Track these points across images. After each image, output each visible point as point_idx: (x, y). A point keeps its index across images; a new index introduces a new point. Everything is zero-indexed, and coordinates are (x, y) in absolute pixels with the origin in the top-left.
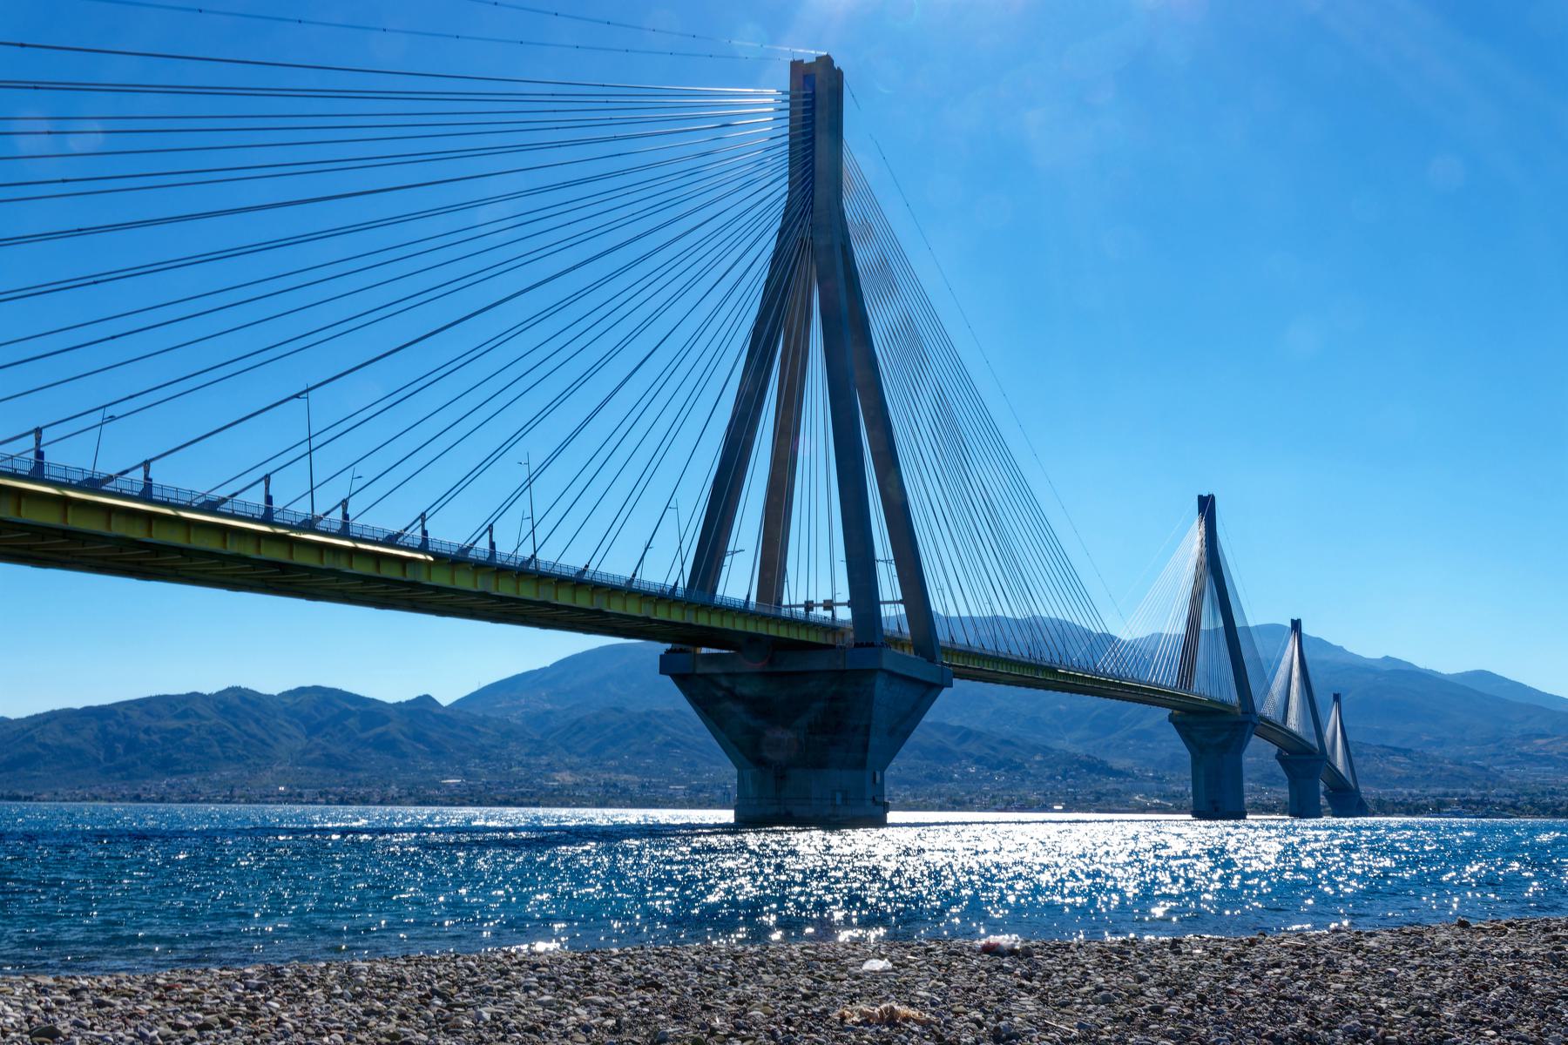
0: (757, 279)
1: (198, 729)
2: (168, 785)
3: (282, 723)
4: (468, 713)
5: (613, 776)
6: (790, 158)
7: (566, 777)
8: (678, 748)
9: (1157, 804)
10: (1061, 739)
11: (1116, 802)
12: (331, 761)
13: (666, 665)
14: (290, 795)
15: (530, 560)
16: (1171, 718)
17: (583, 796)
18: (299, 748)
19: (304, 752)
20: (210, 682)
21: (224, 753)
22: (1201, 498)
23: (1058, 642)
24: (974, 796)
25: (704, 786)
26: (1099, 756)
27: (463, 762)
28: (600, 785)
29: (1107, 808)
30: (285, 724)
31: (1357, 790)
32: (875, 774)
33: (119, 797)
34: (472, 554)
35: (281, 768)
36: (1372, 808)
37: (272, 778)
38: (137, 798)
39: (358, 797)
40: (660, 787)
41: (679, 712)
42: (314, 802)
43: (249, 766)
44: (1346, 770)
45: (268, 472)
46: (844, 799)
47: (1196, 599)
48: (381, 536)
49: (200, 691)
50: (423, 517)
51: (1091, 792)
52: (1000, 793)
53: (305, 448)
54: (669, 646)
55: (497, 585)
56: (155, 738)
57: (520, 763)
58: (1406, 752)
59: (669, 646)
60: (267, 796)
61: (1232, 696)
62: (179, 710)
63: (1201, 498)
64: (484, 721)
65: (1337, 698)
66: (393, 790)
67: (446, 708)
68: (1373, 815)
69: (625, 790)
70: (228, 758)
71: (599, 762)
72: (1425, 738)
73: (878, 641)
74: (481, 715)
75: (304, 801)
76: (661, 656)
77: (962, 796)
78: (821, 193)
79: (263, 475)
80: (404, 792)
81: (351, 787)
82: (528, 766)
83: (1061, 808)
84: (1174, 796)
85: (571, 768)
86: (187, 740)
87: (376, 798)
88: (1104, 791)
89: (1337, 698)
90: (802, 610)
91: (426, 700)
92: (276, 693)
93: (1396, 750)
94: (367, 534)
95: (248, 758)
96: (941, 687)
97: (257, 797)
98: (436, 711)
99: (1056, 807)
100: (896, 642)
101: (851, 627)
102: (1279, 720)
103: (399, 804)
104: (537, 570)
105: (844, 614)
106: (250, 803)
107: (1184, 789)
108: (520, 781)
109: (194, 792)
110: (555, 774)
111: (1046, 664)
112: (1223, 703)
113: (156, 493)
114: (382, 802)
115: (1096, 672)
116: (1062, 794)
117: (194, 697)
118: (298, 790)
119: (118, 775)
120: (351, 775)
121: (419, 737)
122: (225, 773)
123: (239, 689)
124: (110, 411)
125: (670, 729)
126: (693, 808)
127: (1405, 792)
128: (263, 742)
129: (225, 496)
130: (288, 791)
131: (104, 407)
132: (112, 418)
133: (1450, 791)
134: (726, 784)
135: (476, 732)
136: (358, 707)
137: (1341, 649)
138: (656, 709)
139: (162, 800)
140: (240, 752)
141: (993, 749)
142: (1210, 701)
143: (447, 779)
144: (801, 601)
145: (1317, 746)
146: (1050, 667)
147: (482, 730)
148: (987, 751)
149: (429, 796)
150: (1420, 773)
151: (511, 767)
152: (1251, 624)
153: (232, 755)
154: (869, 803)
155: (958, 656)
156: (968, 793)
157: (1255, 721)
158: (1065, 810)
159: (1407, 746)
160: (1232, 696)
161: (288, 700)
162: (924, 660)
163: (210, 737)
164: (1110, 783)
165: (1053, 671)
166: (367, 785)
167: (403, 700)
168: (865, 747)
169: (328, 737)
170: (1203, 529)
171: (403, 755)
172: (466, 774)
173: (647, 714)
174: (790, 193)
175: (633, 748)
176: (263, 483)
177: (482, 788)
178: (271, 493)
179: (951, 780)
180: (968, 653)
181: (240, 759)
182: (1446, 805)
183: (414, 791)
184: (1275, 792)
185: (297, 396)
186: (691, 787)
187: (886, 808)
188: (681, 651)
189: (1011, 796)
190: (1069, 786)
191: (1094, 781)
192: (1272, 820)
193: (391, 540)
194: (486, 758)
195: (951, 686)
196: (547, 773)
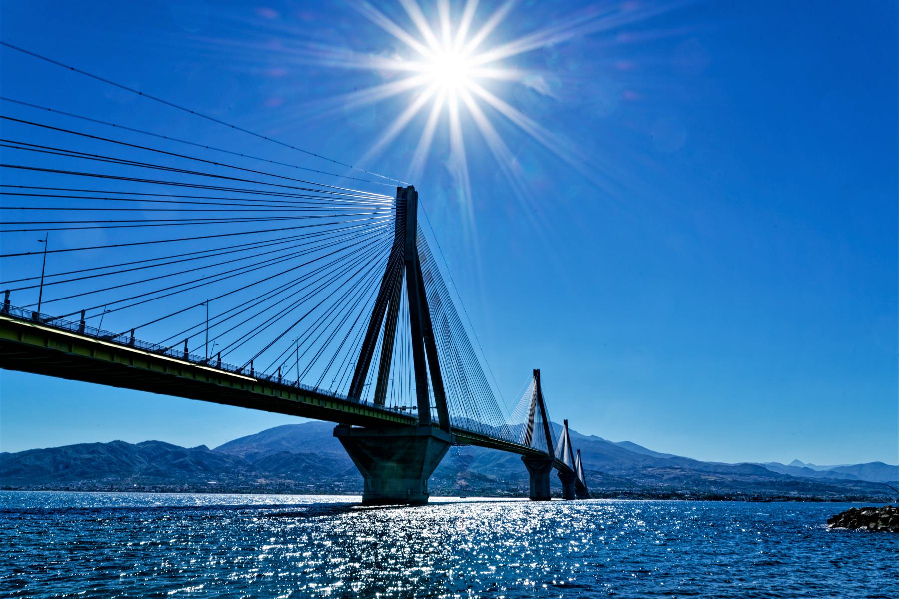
0: (378, 270)
1: (98, 459)
2: (82, 483)
3: (138, 456)
4: (221, 453)
7: (262, 481)
8: (311, 469)
11: (491, 492)
12: (158, 473)
13: (336, 432)
14: (139, 488)
16: (523, 459)
17: (470, 491)
18: (145, 467)
19: (147, 469)
20: (106, 438)
21: (109, 469)
22: (535, 371)
23: (480, 426)
24: (434, 490)
26: (483, 474)
27: (218, 474)
28: (277, 484)
30: (140, 457)
31: (586, 489)
32: (424, 481)
33: (59, 488)
34: (272, 379)
35: (135, 476)
36: (591, 495)
37: (131, 481)
38: (68, 489)
39: (170, 489)
40: (303, 485)
42: (150, 491)
43: (121, 475)
45: (187, 338)
47: (533, 407)
49: (124, 441)
50: (252, 362)
51: (481, 489)
52: (444, 489)
54: (338, 424)
56: (78, 462)
58: (601, 473)
59: (338, 424)
60: (129, 489)
61: (547, 451)
62: (91, 450)
63: (535, 371)
64: (228, 456)
65: (579, 451)
67: (211, 451)
68: (591, 498)
69: (288, 486)
70: (112, 472)
71: (277, 474)
72: (607, 467)
74: (226, 454)
75: (145, 490)
79: (184, 339)
80: (191, 487)
81: (167, 485)
82: (246, 476)
84: (513, 490)
86: (93, 463)
87: (178, 489)
88: (485, 488)
89: (579, 451)
92: (136, 444)
93: (597, 472)
94: (230, 368)
95: (121, 472)
97: (124, 489)
98: (207, 452)
100: (435, 425)
101: (417, 418)
103: (188, 492)
104: (299, 388)
106: (120, 491)
107: (516, 487)
108: (242, 482)
109: (95, 486)
110: (257, 479)
111: (481, 434)
112: (544, 453)
113: (136, 344)
117: (98, 444)
118: (143, 486)
119: (59, 479)
120: (167, 479)
121: (199, 463)
122: (109, 478)
123: (119, 441)
124: (108, 308)
125: (309, 461)
127: (601, 489)
128: (128, 464)
130: (138, 486)
131: (106, 305)
132: (109, 311)
135: (224, 461)
136: (173, 450)
138: (302, 452)
139: (79, 490)
140: (117, 469)
142: (540, 452)
143: (210, 481)
144: (392, 407)
147: (227, 460)
148: (439, 471)
150: (606, 481)
151: (238, 476)
152: (552, 421)
153: (113, 470)
154: (421, 494)
157: (555, 460)
159: (601, 470)
160: (547, 451)
161: (141, 447)
163: (104, 462)
164: (488, 485)
166: (175, 484)
167: (193, 447)
168: (421, 469)
169: (158, 463)
171: (191, 471)
173: (299, 454)
174: (395, 239)
176: (184, 343)
177: (226, 486)
178: (187, 348)
181: (117, 472)
182: (618, 494)
186: (316, 486)
187: (428, 495)
191: (481, 484)
193: (238, 372)
196: (255, 479)
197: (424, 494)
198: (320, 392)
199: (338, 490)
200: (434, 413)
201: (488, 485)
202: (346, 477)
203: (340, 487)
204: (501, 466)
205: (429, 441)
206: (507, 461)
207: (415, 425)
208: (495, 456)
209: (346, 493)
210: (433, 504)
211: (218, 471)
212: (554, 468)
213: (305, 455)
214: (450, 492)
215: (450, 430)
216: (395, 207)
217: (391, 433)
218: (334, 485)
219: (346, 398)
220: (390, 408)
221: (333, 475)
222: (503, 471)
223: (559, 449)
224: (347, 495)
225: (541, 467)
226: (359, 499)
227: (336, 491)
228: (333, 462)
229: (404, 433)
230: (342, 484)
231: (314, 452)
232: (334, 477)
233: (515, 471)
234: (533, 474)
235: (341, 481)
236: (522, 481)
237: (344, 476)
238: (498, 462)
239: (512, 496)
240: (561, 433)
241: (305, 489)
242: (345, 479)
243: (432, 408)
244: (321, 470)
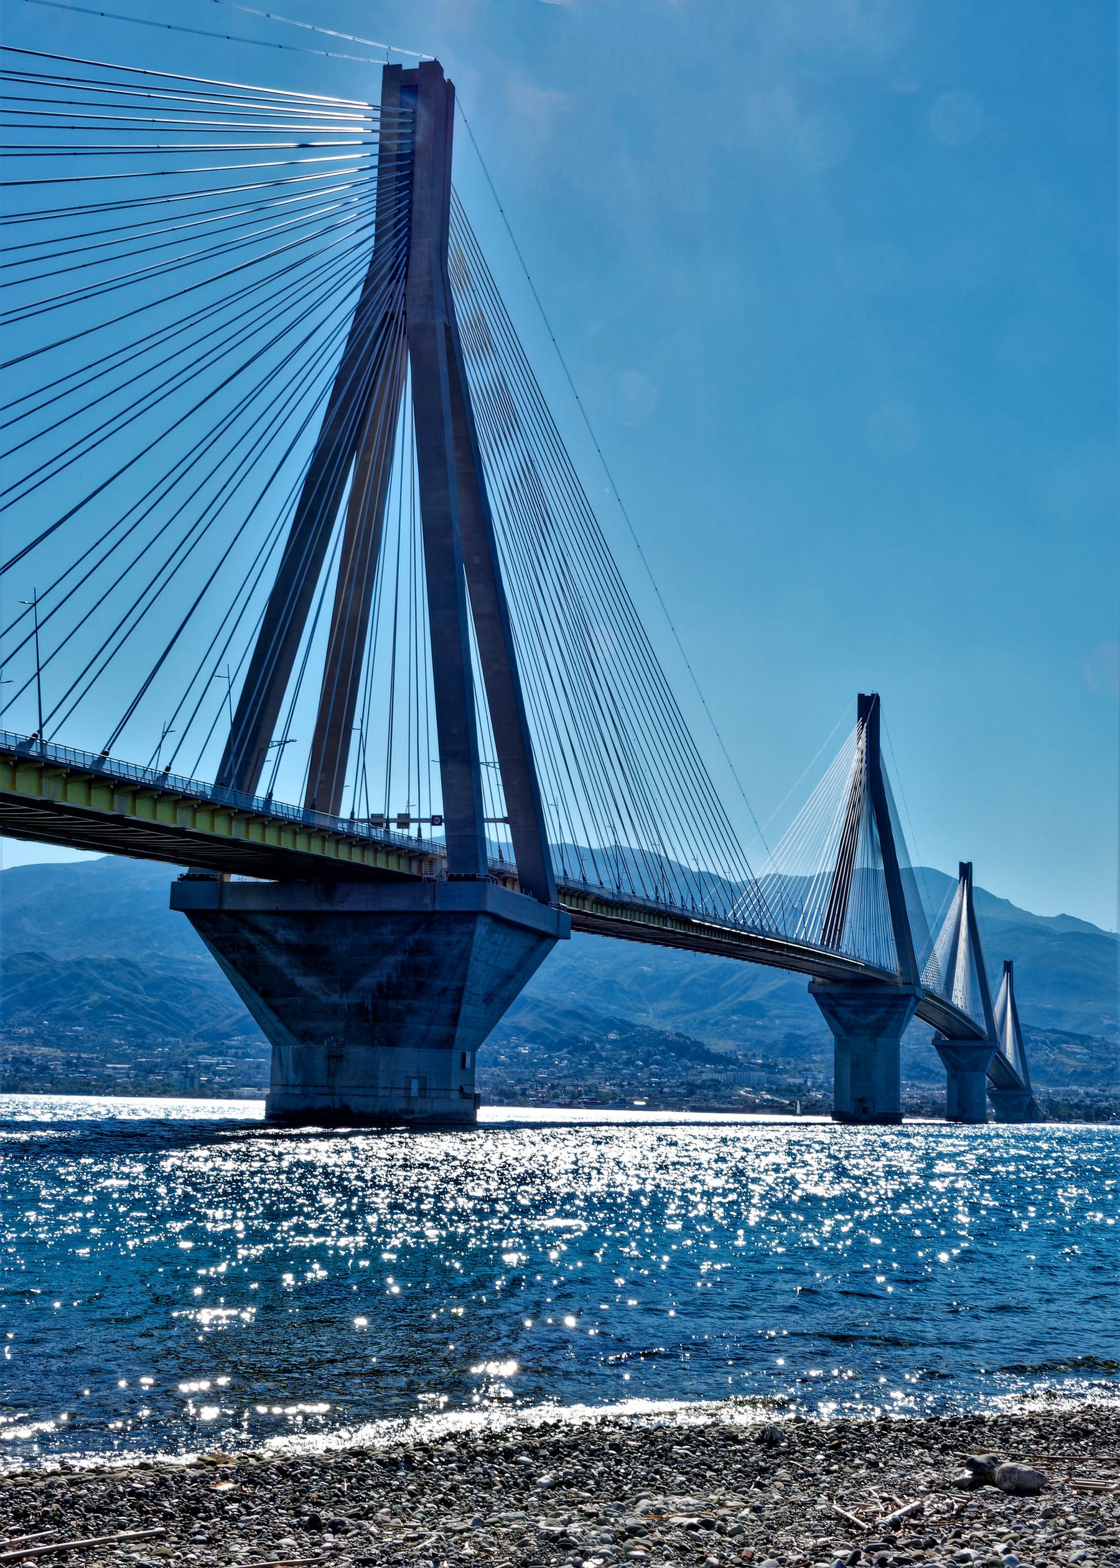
6: (378, 202)
8: (120, 1011)
9: (767, 1100)
10: (644, 1011)
11: (715, 1097)
13: (179, 898)
22: (861, 698)
24: (526, 1086)
25: (156, 1065)
26: (693, 1035)
29: (704, 1104)
44: (1016, 1062)
46: (422, 1089)
47: (851, 829)
51: (682, 1084)
52: (561, 1082)
54: (184, 870)
59: (184, 870)
61: (891, 961)
63: (861, 698)
65: (1008, 967)
73: (482, 874)
76: (173, 884)
77: (512, 1086)
78: (422, 250)
83: (644, 1103)
84: (790, 1091)
89: (1008, 967)
90: (345, 826)
96: (555, 938)
99: (636, 1103)
100: (502, 877)
101: (444, 853)
102: (939, 991)
107: (801, 1081)
112: (881, 970)
116: (644, 1085)
125: (111, 986)
126: (141, 1095)
134: (186, 1062)
137: (1006, 903)
141: (554, 1022)
142: (867, 967)
145: (984, 1027)
146: (683, 916)
152: (915, 863)
154: (455, 1095)
155: (571, 897)
156: (519, 1081)
157: (919, 994)
158: (648, 1107)
160: (891, 961)
162: (535, 900)
164: (708, 1072)
165: (685, 921)
168: (455, 1017)
170: (862, 744)
174: (376, 251)
179: (496, 1063)
180: (580, 894)
184: (920, 1088)
186: (138, 1066)
187: (478, 1101)
188: (202, 878)
189: (577, 1086)
191: (686, 1068)
192: (919, 1125)
195: (568, 938)
197: (464, 1096)
198: (115, 768)
199: (209, 1081)
200: (499, 835)
201: (708, 1072)
202: (236, 1041)
203: (215, 1073)
204: (752, 1009)
205: (482, 928)
206: (774, 995)
207: (434, 876)
208: (735, 978)
209: (235, 1091)
210: (491, 1128)
211: (988, 1099)
212: (916, 1021)
213: (99, 966)
214: (580, 1094)
215: (553, 894)
216: (376, 137)
217: (356, 900)
218: (198, 1066)
219: (209, 792)
220: (352, 820)
221: (193, 1032)
222: (757, 1026)
223: (936, 961)
224: (240, 1097)
225: (872, 1018)
226: (256, 1110)
227: (202, 1086)
228: (194, 991)
229: (399, 901)
230: (225, 1063)
231: (128, 955)
232: (195, 1038)
233: (800, 1028)
234: (845, 1037)
235: (220, 1054)
236: (822, 1062)
237: (228, 1036)
238: (742, 999)
239: (783, 1110)
240: (947, 908)
241: (100, 1076)
242: (230, 1048)
243: (495, 820)
244: (153, 1017)
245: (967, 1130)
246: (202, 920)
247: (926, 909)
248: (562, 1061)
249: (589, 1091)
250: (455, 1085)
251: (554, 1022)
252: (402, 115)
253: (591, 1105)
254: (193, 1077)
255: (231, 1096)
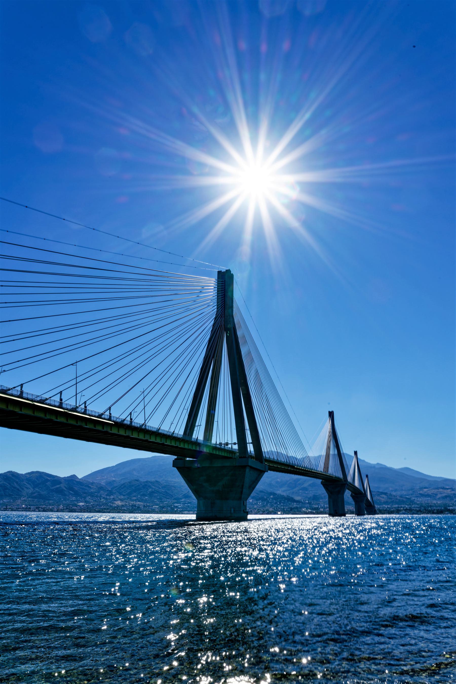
5: (134, 503)
7: (119, 503)
13: (175, 464)
15: (143, 425)
22: (329, 412)
25: (165, 506)
26: (290, 496)
27: (85, 498)
41: (156, 481)
48: (97, 415)
53: (74, 382)
54: (176, 457)
55: (132, 434)
57: (104, 498)
58: (385, 494)
59: (176, 457)
61: (341, 476)
63: (329, 412)
64: (92, 484)
65: (367, 476)
66: (61, 507)
67: (80, 479)
69: (138, 507)
72: (391, 489)
73: (247, 456)
80: (65, 508)
81: (47, 506)
82: (106, 499)
84: (315, 509)
85: (121, 500)
87: (56, 509)
89: (367, 476)
91: (74, 476)
94: (94, 414)
98: (77, 480)
100: (251, 457)
101: (238, 451)
103: (63, 512)
104: (145, 429)
105: (236, 447)
114: (58, 511)
115: (300, 466)
120: (47, 501)
121: (71, 489)
125: (154, 487)
127: (386, 507)
129: (48, 398)
133: (400, 506)
135: (90, 487)
141: (257, 493)
142: (336, 477)
144: (218, 443)
147: (92, 487)
149: (73, 509)
151: (101, 499)
154: (242, 512)
159: (385, 491)
160: (341, 476)
164: (295, 505)
165: (293, 467)
166: (53, 505)
168: (242, 492)
172: (86, 502)
173: (147, 482)
175: (141, 493)
177: (91, 507)
182: (400, 511)
183: (68, 507)
185: (72, 364)
186: (160, 507)
187: (247, 513)
190: (282, 506)
191: (290, 504)
194: (92, 496)
198: (162, 432)
200: (251, 448)
201: (295, 505)
203: (178, 508)
204: (305, 489)
205: (247, 470)
206: (310, 485)
210: (251, 520)
213: (151, 482)
218: (174, 506)
221: (173, 498)
224: (185, 514)
226: (194, 517)
227: (175, 511)
228: (173, 488)
229: (227, 463)
237: (181, 499)
238: (302, 486)
239: (314, 514)
241: (151, 509)
243: (249, 443)
244: (164, 494)
245: (362, 517)
246: (179, 469)
247: (348, 464)
248: (260, 503)
249: (267, 510)
250: (242, 509)
251: (257, 493)
252: (222, 281)
253: (268, 514)
254: (173, 509)
255: (182, 514)
